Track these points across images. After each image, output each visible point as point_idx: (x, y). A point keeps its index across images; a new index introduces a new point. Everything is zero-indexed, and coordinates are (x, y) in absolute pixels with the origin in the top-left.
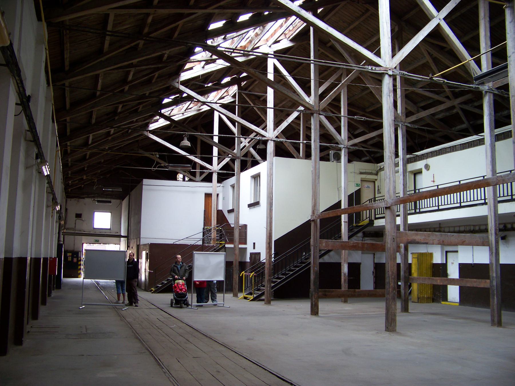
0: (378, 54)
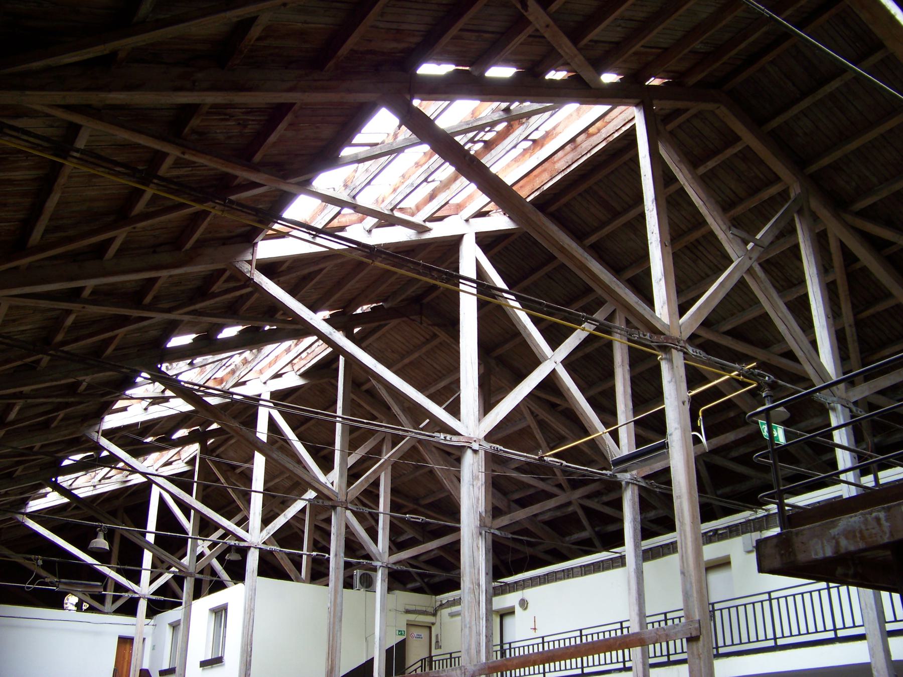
0: (454, 410)
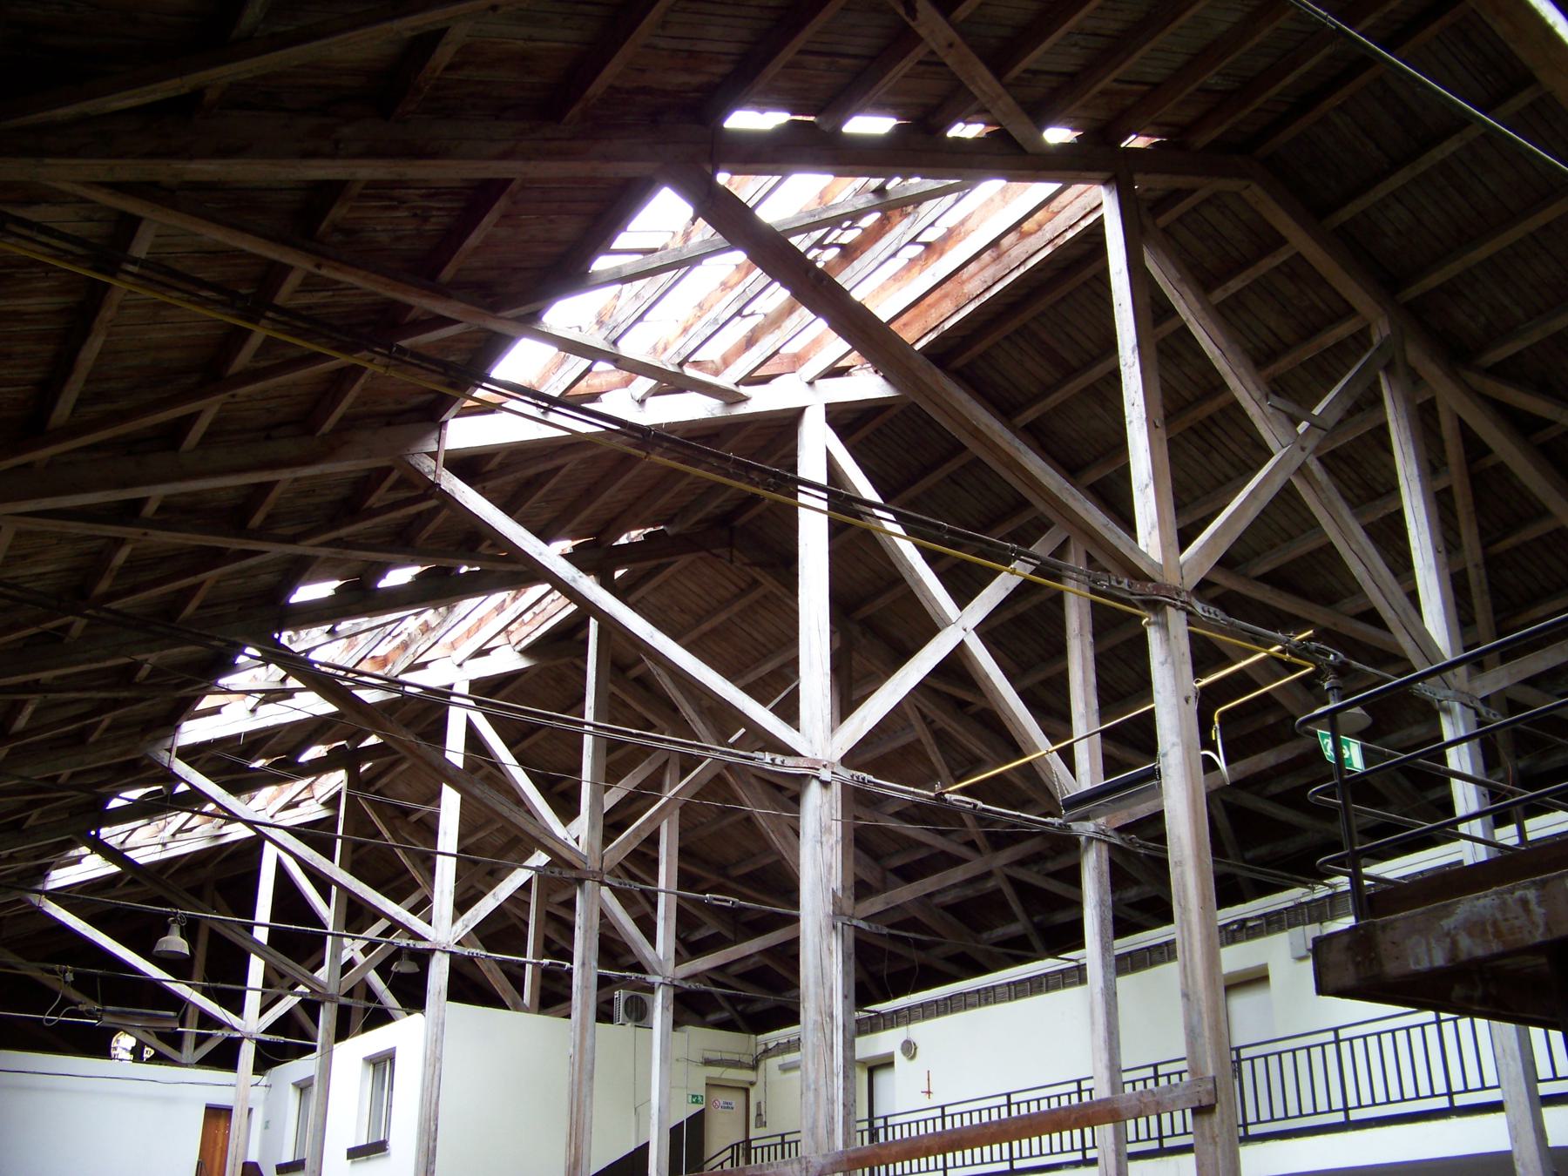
0: (789, 712)
